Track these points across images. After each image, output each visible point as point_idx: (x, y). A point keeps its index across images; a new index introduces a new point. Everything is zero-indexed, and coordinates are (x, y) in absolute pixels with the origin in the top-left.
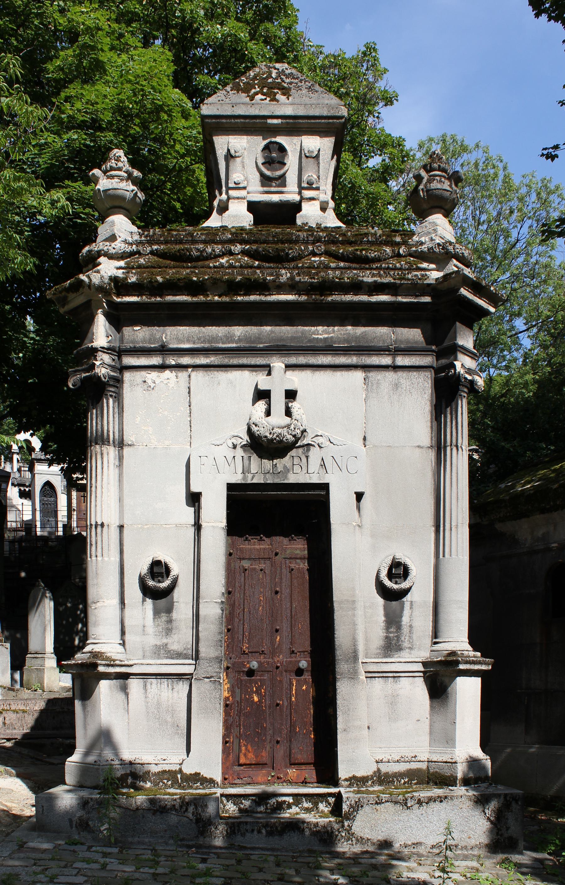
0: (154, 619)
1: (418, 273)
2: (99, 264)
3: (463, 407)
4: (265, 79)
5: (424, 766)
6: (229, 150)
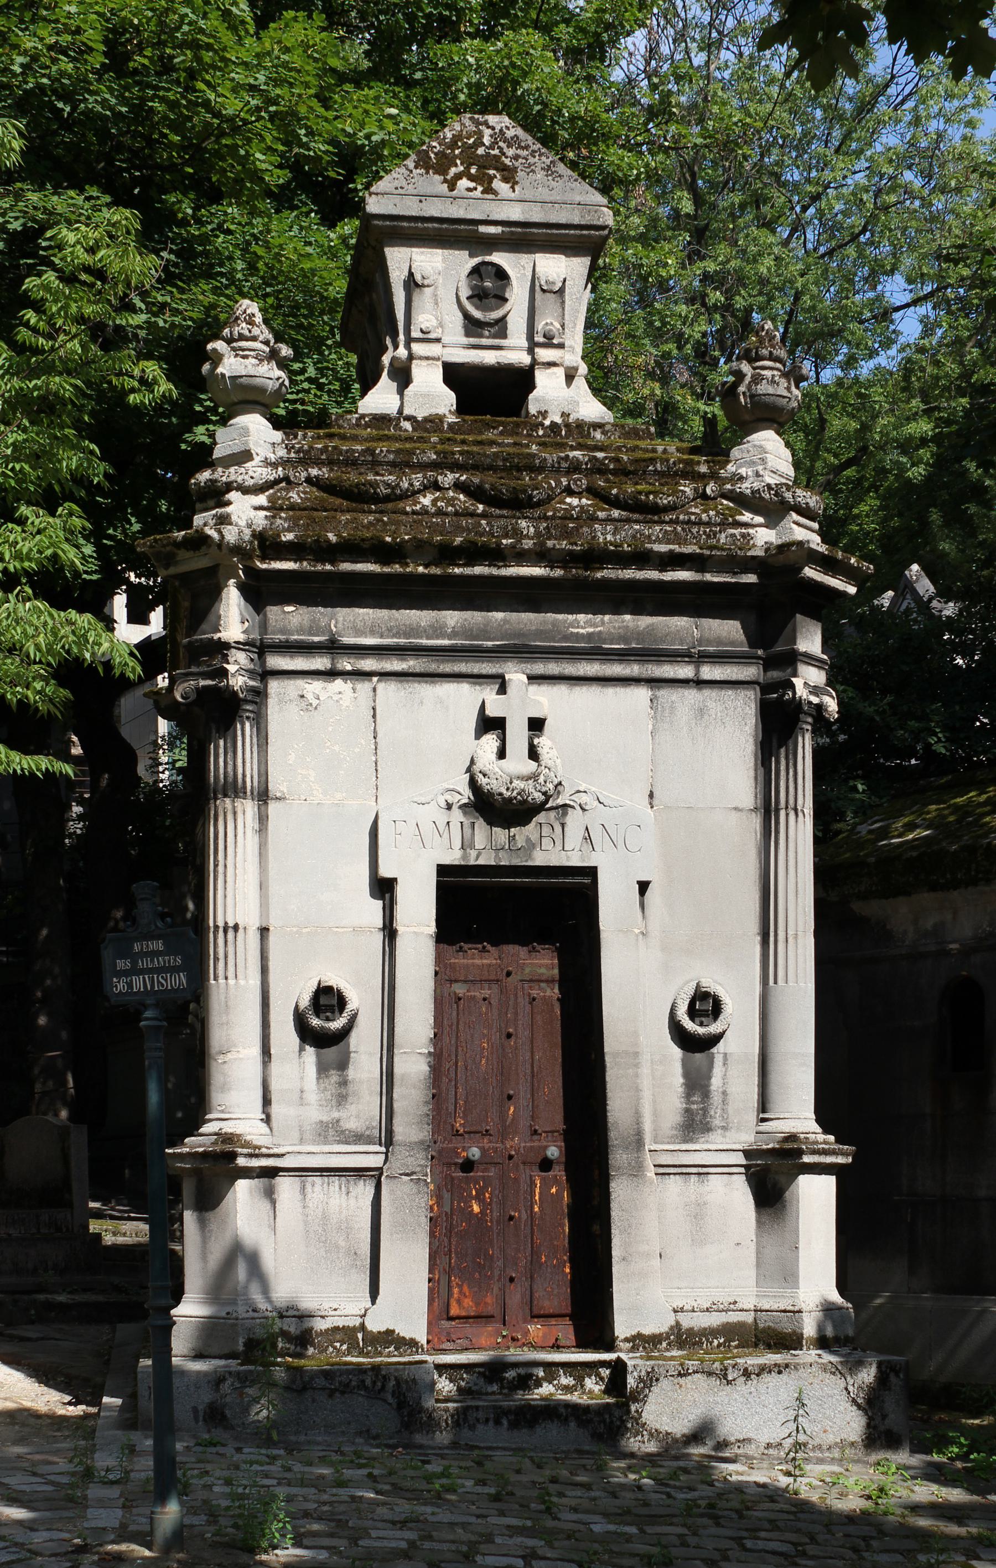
0: (318, 1079)
1: (736, 532)
2: (229, 503)
3: (805, 745)
4: (471, 147)
5: (749, 1318)
6: (411, 274)
